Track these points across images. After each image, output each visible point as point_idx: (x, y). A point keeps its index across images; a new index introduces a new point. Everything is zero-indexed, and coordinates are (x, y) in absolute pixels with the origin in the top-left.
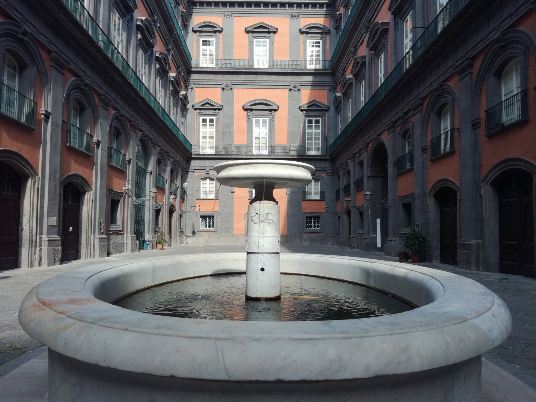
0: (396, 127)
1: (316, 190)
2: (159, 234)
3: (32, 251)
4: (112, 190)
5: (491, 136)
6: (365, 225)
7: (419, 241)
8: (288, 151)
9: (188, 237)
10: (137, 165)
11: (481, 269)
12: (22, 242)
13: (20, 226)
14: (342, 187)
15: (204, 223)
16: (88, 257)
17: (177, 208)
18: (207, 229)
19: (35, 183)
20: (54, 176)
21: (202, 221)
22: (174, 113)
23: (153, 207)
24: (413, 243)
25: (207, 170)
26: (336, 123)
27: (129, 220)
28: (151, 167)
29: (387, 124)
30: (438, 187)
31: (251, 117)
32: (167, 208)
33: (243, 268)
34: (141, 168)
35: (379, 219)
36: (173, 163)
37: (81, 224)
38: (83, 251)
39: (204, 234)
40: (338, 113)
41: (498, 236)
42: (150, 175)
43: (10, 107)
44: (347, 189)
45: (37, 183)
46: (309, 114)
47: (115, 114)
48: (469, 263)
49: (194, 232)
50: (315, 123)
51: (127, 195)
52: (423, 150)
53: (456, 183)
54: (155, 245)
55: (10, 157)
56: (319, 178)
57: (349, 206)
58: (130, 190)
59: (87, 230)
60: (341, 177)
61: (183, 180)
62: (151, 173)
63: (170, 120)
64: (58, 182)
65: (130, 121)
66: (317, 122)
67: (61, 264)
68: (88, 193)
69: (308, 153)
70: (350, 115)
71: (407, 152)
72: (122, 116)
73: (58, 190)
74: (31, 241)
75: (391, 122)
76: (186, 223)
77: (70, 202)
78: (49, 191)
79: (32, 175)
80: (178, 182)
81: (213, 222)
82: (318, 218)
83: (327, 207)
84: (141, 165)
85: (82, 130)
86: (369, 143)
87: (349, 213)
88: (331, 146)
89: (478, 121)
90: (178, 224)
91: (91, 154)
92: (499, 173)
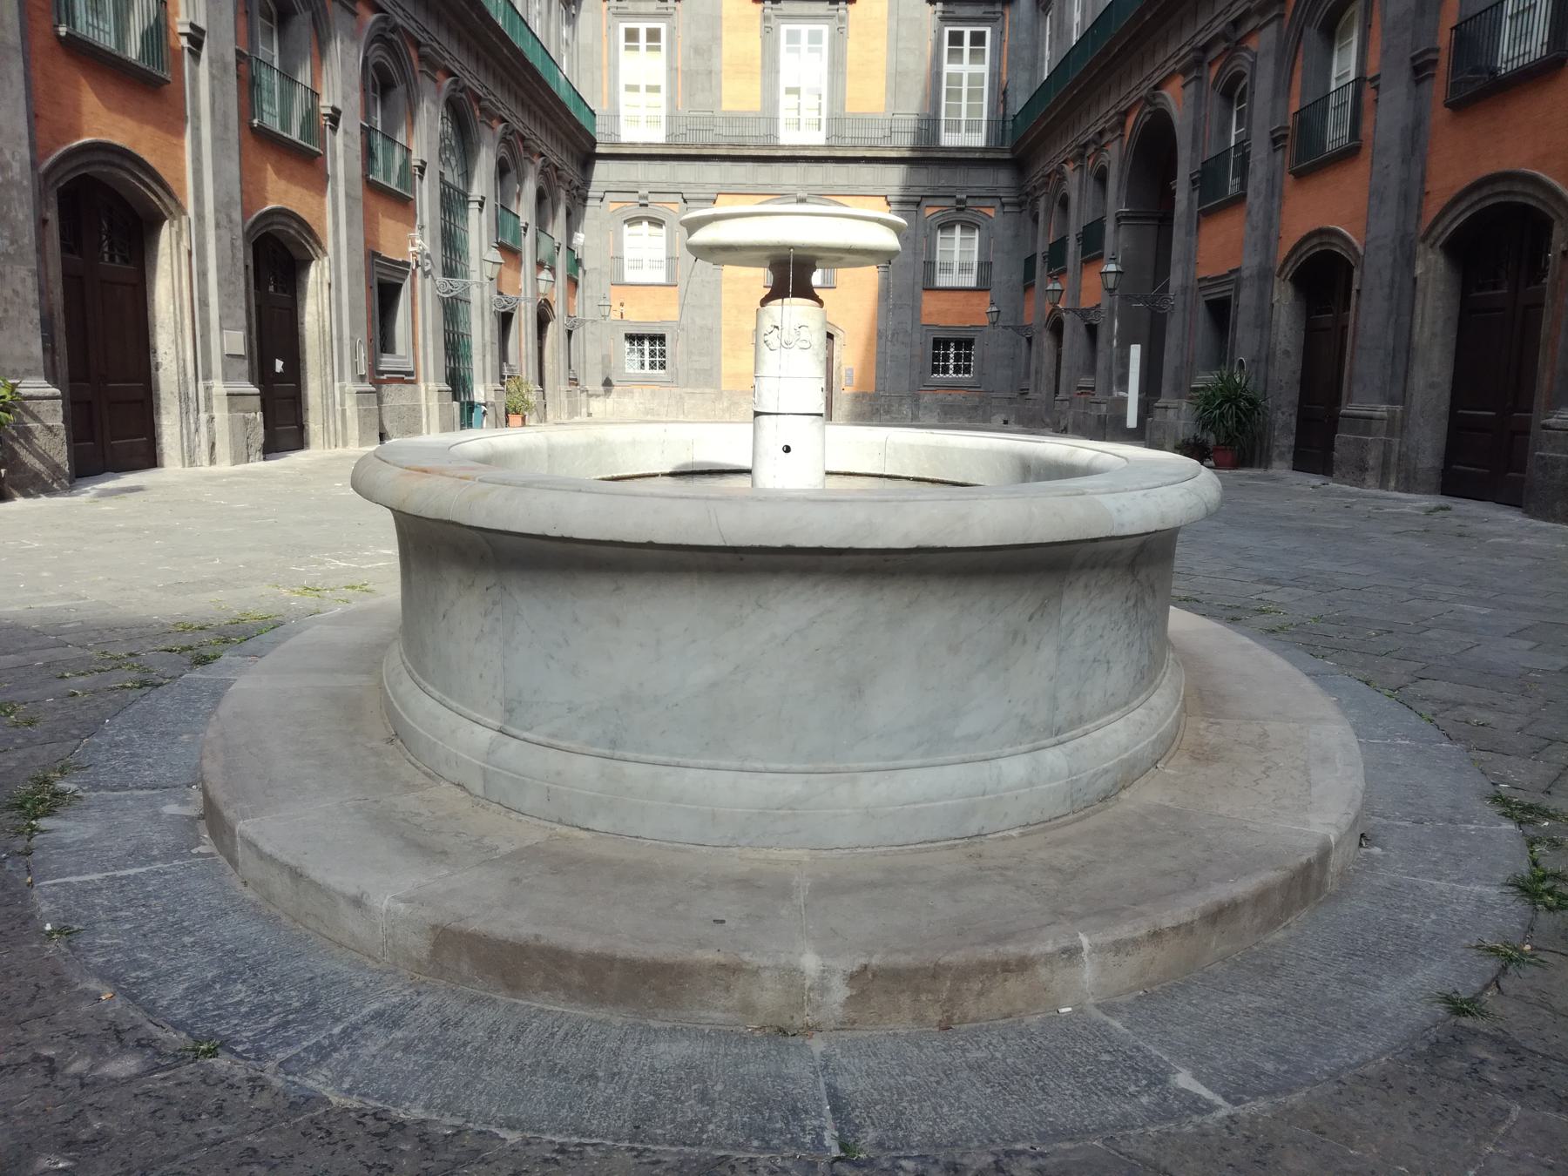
0: (1206, 65)
1: (965, 260)
2: (513, 386)
3: (188, 423)
4: (378, 255)
5: (1461, 104)
6: (1100, 365)
7: (1238, 407)
8: (887, 132)
9: (591, 396)
10: (442, 181)
11: (1392, 484)
12: (159, 399)
13: (151, 355)
14: (1042, 248)
15: (636, 357)
16: (329, 443)
17: (558, 309)
18: (646, 375)
19: (179, 234)
20: (229, 216)
21: (632, 351)
22: (540, 13)
23: (491, 307)
24: (1222, 415)
25: (643, 192)
26: (1036, 46)
27: (430, 343)
28: (482, 183)
29: (1182, 53)
30: (1306, 252)
31: (774, 22)
32: (529, 308)
33: (747, 464)
34: (455, 189)
35: (1139, 346)
36: (542, 172)
37: (304, 352)
38: (314, 425)
39: (637, 390)
40: (1044, 10)
41: (1447, 395)
42: (481, 211)
43: (100, 17)
44: (1056, 256)
45: (185, 236)
46: (953, 12)
47: (374, 23)
48: (1363, 469)
49: (607, 383)
50: (972, 44)
51: (419, 271)
52: (1275, 141)
53: (1354, 240)
54: (503, 416)
55: (113, 165)
56: (977, 220)
57: (1060, 306)
58: (428, 256)
59: (323, 369)
60: (1041, 218)
61: (572, 224)
62: (481, 204)
63: (530, 36)
64: (239, 232)
65: (418, 45)
66: (978, 39)
67: (265, 459)
68: (317, 265)
69: (948, 139)
70: (1077, 17)
71: (1233, 144)
72: (395, 29)
73: (240, 255)
74: (184, 398)
75: (1193, 49)
76: (585, 356)
77: (271, 289)
78: (217, 259)
79: (171, 213)
80: (558, 229)
81: (663, 354)
82: (969, 343)
83: (995, 309)
84: (452, 177)
85: (288, 77)
86: (1126, 113)
87: (1057, 328)
88: (1018, 118)
89: (1431, 56)
90: (562, 356)
91: (317, 150)
92: (1468, 214)
